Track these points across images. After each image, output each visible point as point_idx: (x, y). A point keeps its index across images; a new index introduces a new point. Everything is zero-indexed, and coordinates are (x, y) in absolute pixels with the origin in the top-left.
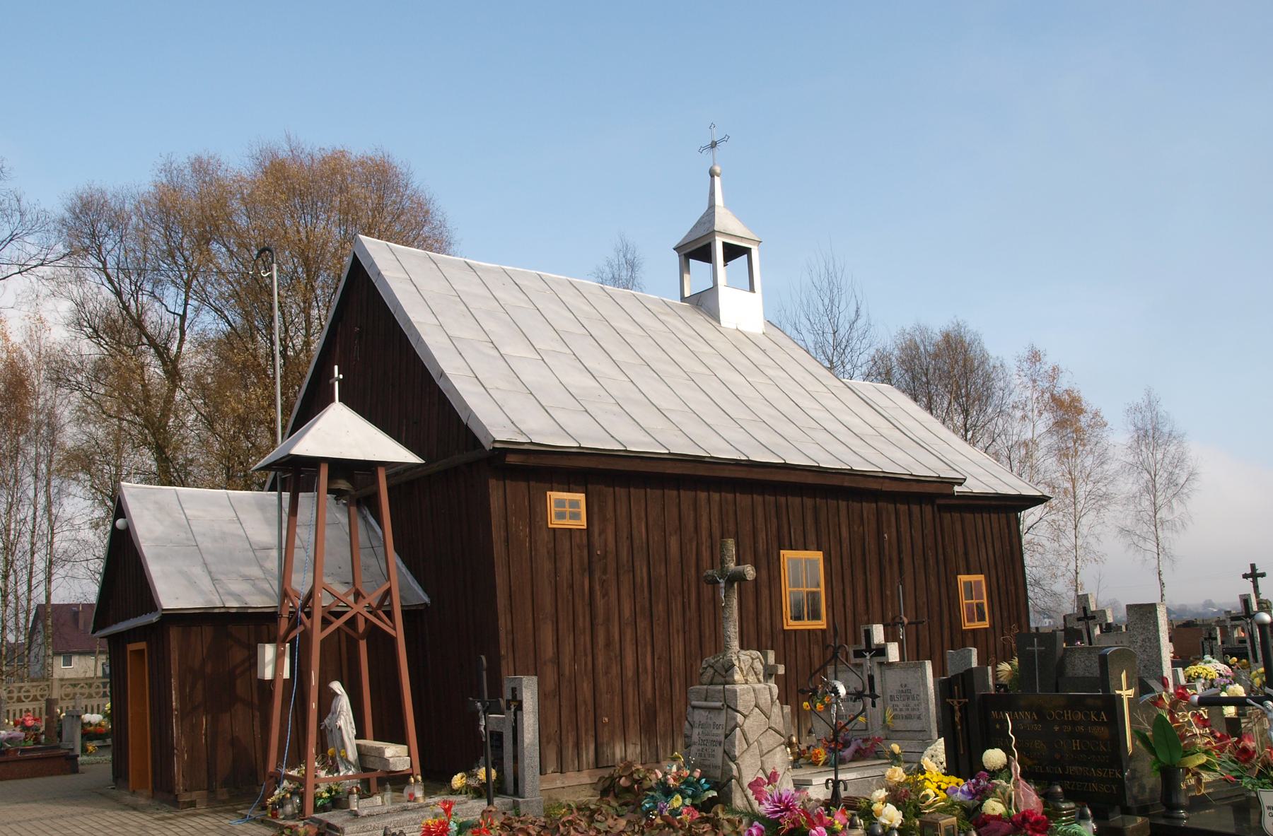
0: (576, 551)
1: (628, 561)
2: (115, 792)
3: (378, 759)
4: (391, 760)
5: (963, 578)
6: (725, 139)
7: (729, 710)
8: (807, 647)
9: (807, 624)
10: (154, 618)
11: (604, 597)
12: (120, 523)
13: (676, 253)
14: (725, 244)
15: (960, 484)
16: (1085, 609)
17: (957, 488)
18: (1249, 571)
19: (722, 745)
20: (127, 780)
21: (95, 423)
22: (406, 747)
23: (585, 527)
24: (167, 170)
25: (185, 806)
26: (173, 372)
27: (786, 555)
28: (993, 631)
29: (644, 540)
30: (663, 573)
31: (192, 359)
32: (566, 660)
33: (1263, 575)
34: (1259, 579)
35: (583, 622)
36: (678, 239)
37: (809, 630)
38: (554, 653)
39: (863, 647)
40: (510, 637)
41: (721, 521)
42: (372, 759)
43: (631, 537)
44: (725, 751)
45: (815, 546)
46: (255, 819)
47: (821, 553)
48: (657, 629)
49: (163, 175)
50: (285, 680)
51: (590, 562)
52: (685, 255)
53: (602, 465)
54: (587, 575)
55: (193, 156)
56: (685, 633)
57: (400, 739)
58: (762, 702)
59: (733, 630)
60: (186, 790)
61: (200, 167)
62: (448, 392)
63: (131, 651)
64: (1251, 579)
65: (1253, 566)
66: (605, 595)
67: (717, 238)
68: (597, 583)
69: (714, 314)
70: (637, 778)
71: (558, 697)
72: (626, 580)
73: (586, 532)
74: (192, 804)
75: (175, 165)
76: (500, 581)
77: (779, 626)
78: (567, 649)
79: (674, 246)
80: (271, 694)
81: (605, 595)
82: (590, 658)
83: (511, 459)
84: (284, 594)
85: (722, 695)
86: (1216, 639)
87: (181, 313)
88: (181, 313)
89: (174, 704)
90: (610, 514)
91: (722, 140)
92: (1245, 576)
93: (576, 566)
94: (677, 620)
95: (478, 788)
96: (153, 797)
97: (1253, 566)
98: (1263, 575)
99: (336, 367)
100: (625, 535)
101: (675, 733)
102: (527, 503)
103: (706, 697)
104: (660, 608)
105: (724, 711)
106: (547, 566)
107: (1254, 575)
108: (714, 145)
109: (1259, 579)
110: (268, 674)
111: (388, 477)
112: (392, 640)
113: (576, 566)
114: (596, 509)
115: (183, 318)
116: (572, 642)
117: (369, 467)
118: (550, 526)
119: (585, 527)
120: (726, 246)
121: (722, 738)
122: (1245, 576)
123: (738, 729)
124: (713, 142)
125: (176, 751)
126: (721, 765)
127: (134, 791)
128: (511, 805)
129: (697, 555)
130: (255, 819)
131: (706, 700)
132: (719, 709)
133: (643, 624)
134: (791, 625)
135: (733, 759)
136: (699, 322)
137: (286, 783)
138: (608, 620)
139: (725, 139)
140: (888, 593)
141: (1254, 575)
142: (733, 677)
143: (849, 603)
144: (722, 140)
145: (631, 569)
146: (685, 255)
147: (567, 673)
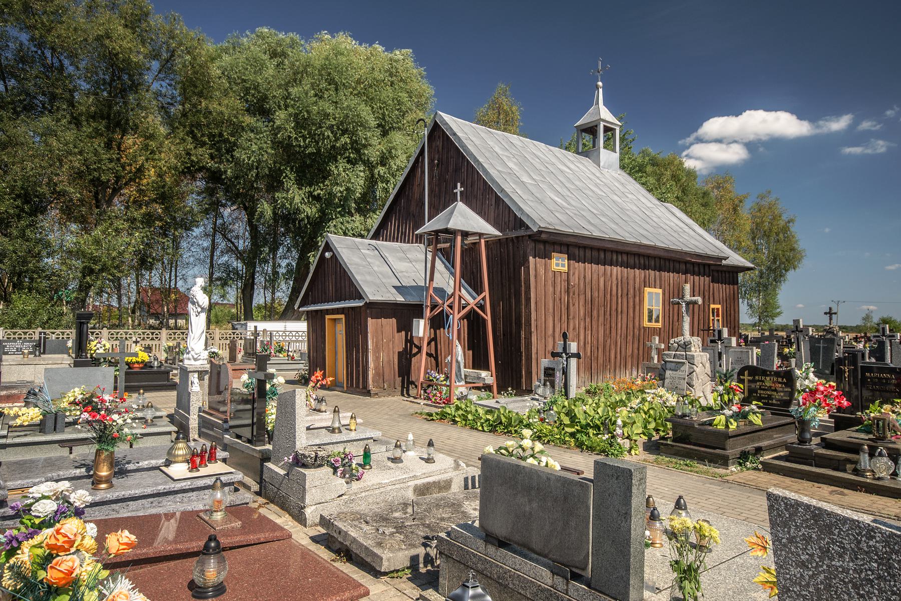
0: (563, 283)
5: (712, 306)
9: (653, 325)
14: (604, 126)
15: (725, 260)
16: (797, 327)
17: (724, 262)
21: (141, 179)
27: (647, 290)
35: (564, 317)
39: (717, 338)
48: (594, 323)
57: (487, 368)
59: (686, 327)
72: (582, 297)
83: (543, 236)
86: (840, 345)
92: (826, 313)
93: (563, 290)
94: (601, 319)
104: (595, 313)
106: (551, 289)
107: (830, 313)
110: (421, 334)
112: (484, 321)
113: (563, 290)
133: (588, 320)
134: (646, 324)
135: (692, 386)
138: (574, 318)
141: (830, 313)
143: (671, 316)
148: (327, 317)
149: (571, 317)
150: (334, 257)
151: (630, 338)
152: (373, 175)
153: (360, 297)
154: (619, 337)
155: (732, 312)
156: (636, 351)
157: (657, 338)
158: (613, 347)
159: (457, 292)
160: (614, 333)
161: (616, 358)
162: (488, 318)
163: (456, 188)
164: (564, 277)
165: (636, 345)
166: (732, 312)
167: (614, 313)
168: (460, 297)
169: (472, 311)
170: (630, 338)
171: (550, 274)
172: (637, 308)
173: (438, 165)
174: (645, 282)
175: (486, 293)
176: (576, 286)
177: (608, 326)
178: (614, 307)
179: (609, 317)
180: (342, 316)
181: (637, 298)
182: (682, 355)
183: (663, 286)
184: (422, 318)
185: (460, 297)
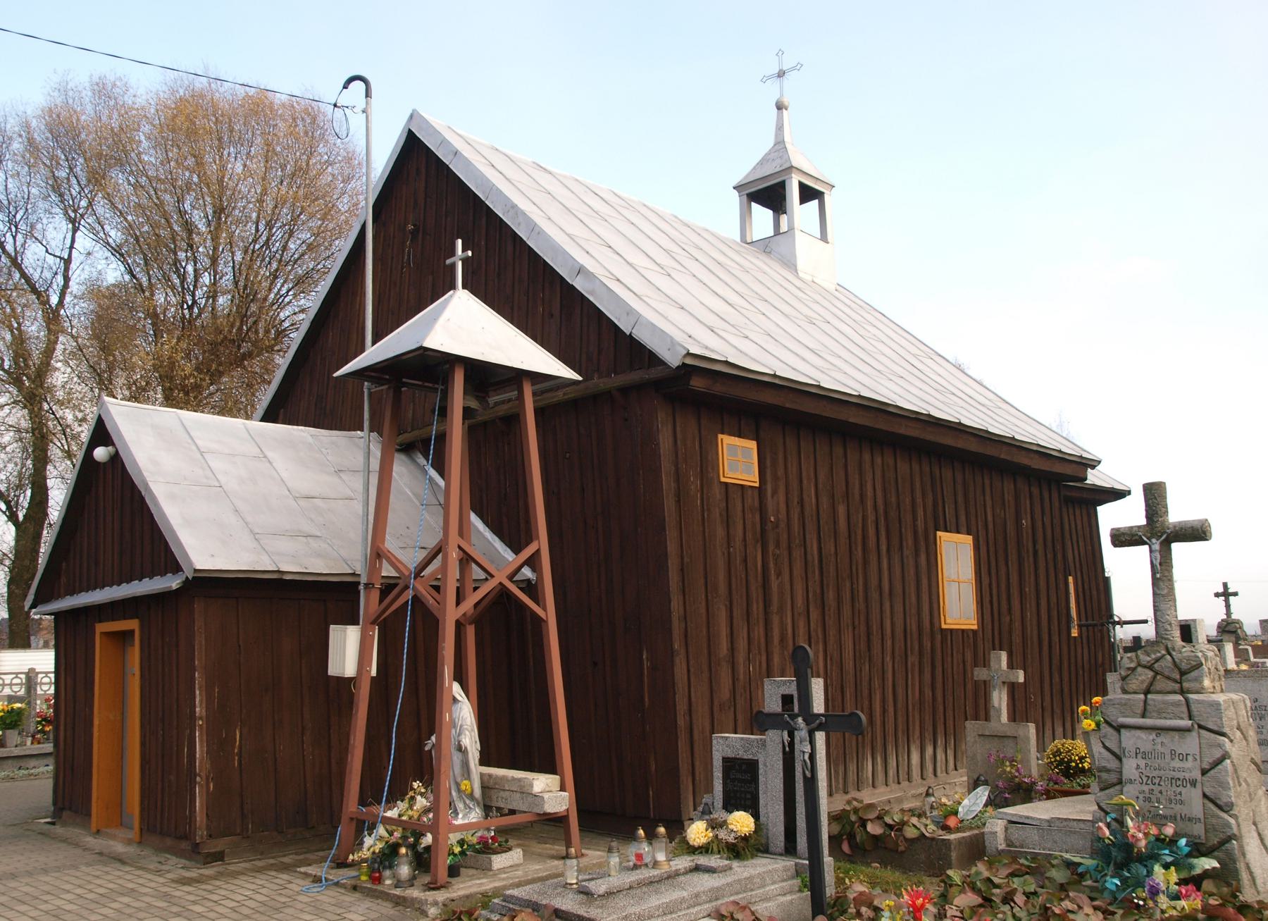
0: (749, 516)
1: (799, 533)
2: (58, 830)
3: (518, 795)
4: (546, 796)
6: (798, 67)
7: (1203, 732)
8: (961, 651)
10: (172, 582)
11: (778, 578)
12: (100, 453)
13: (736, 193)
14: (802, 185)
18: (1221, 590)
19: (1198, 785)
20: (89, 815)
22: (558, 777)
23: (757, 485)
24: (64, 90)
25: (209, 860)
26: (53, 318)
28: (1080, 640)
29: (814, 507)
30: (833, 549)
31: (76, 310)
32: (741, 657)
33: (1235, 594)
34: (1231, 598)
35: (757, 608)
36: (739, 175)
37: (963, 631)
38: (728, 650)
40: (683, 625)
41: (884, 490)
42: (502, 794)
43: (801, 502)
44: (1205, 796)
45: (965, 529)
46: (337, 884)
47: (970, 538)
49: (56, 94)
50: (372, 678)
51: (763, 531)
52: (748, 195)
53: (790, 403)
54: (759, 545)
55: (95, 79)
56: (854, 628)
57: (549, 766)
58: (1242, 726)
60: (210, 836)
61: (102, 90)
62: (592, 293)
63: (102, 633)
64: (1223, 598)
65: (1225, 585)
66: (779, 574)
67: (793, 175)
68: (771, 559)
69: (790, 263)
70: (891, 822)
71: (732, 709)
72: (797, 554)
73: (756, 493)
74: (219, 857)
75: (71, 85)
76: (672, 548)
77: (937, 625)
78: (742, 644)
79: (735, 183)
80: (351, 701)
81: (779, 574)
82: (764, 658)
83: (697, 383)
84: (378, 554)
85: (1184, 709)
87: (66, 257)
88: (66, 257)
89: (197, 709)
90: (781, 472)
91: (793, 69)
92: (1217, 595)
93: (749, 535)
95: (733, 844)
96: (140, 843)
97: (1225, 585)
98: (1235, 594)
99: (459, 242)
100: (796, 500)
101: (848, 757)
102: (697, 448)
103: (1144, 713)
104: (831, 595)
105: (1194, 734)
106: (720, 532)
108: (781, 74)
109: (1231, 598)
110: (350, 670)
111: (534, 394)
112: (539, 622)
113: (749, 535)
114: (768, 463)
115: (68, 262)
116: (746, 636)
117: (517, 377)
118: (723, 479)
119: (757, 485)
120: (803, 187)
121: (1196, 774)
122: (1217, 595)
123: (1228, 761)
124: (780, 70)
125: (198, 779)
126: (1201, 816)
127: (98, 831)
128: (793, 871)
129: (863, 531)
130: (337, 884)
131: (1143, 716)
132: (1189, 730)
133: (815, 615)
135: (1226, 808)
136: (769, 268)
137: (381, 830)
138: (781, 609)
139: (798, 67)
140: (1027, 589)
142: (1201, 682)
144: (793, 69)
145: (802, 543)
146: (748, 195)
147: (741, 677)
148: (101, 628)
149: (774, 607)
150: (116, 459)
151: (913, 659)
152: (299, 312)
153: (176, 568)
154: (888, 659)
155: (1094, 592)
156: (928, 692)
157: (1004, 656)
158: (876, 683)
159: (454, 540)
160: (876, 649)
161: (884, 711)
162: (549, 614)
163: (452, 253)
164: (752, 500)
165: (927, 676)
166: (1094, 592)
167: (874, 595)
168: (466, 560)
169: (502, 598)
170: (913, 659)
171: (717, 493)
172: (925, 582)
173: (414, 234)
174: (936, 518)
175: (541, 543)
176: (783, 525)
177: (863, 628)
178: (874, 582)
179: (862, 607)
180: (133, 624)
181: (923, 557)
182: (1176, 704)
183: (974, 529)
184: (355, 622)
185: (466, 560)
